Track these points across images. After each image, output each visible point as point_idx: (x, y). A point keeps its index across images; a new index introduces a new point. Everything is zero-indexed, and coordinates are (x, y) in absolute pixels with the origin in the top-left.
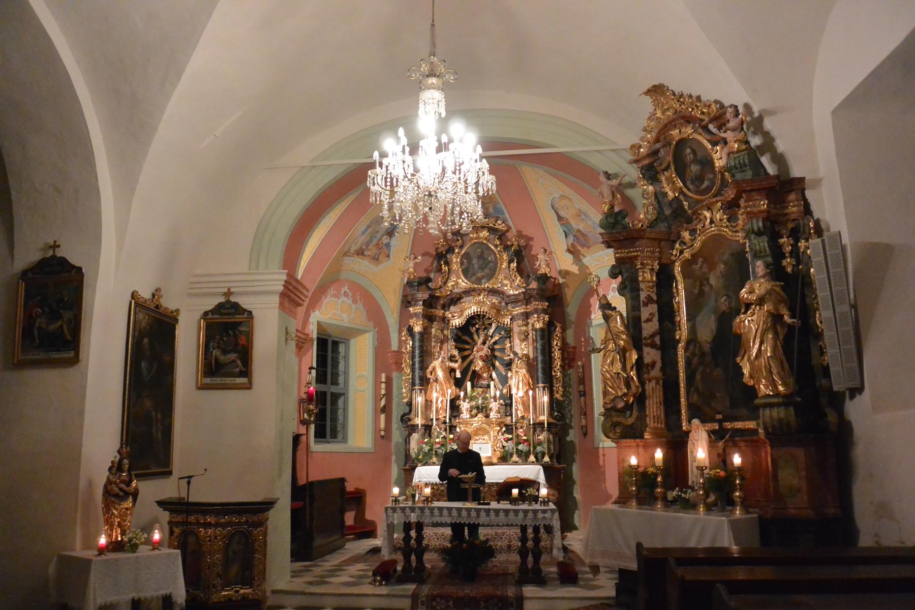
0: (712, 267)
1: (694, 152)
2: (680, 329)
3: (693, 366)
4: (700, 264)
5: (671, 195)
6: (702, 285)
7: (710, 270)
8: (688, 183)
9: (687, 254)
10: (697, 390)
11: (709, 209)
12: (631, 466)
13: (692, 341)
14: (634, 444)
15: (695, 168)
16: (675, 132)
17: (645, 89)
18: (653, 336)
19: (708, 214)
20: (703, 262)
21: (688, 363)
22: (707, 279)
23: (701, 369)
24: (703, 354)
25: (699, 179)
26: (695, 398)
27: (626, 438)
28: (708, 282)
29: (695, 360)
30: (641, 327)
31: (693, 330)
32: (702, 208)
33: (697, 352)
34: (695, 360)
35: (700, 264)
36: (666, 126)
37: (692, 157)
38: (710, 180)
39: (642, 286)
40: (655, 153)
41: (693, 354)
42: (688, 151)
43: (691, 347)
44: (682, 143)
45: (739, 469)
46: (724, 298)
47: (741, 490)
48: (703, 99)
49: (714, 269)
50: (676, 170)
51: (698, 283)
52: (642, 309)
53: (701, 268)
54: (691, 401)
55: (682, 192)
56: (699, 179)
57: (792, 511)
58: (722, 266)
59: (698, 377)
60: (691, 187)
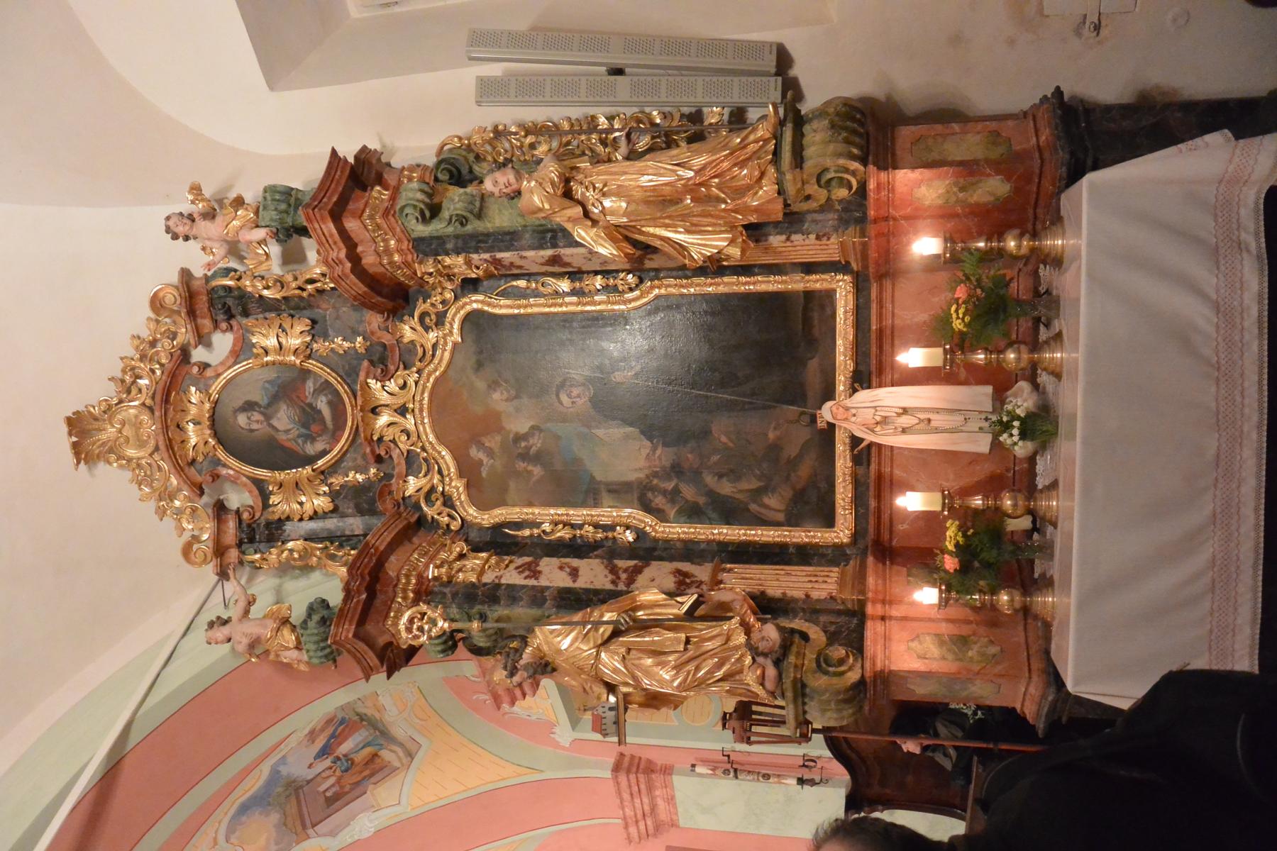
0: (492, 422)
1: (249, 406)
2: (612, 528)
3: (702, 500)
4: (481, 455)
5: (322, 503)
6: (524, 456)
7: (500, 430)
8: (311, 449)
9: (457, 487)
10: (757, 494)
11: (375, 411)
12: (944, 602)
13: (641, 494)
14: (880, 627)
15: (284, 420)
16: (193, 435)
17: (73, 467)
18: (613, 570)
19: (383, 419)
20: (481, 445)
21: (693, 513)
22: (518, 438)
23: (710, 480)
24: (676, 470)
25: (309, 417)
26: (772, 501)
27: (861, 638)
28: (524, 437)
29: (689, 492)
30: (587, 591)
31: (620, 492)
32: (368, 425)
33: (670, 486)
34: (689, 492)
35: (481, 455)
36: (170, 445)
37: (257, 416)
38: (318, 392)
39: (488, 578)
40: (220, 509)
41: (674, 495)
42: (242, 419)
43: (659, 501)
44: (216, 424)
45: (949, 239)
46: (564, 398)
47: (1001, 236)
48: (146, 334)
49: (497, 416)
50: (272, 467)
51: (521, 465)
52: (543, 582)
53: (490, 453)
54: (781, 517)
55: (324, 474)
56: (309, 417)
57: (1043, 138)
58: (496, 396)
59: (726, 488)
60: (320, 446)
